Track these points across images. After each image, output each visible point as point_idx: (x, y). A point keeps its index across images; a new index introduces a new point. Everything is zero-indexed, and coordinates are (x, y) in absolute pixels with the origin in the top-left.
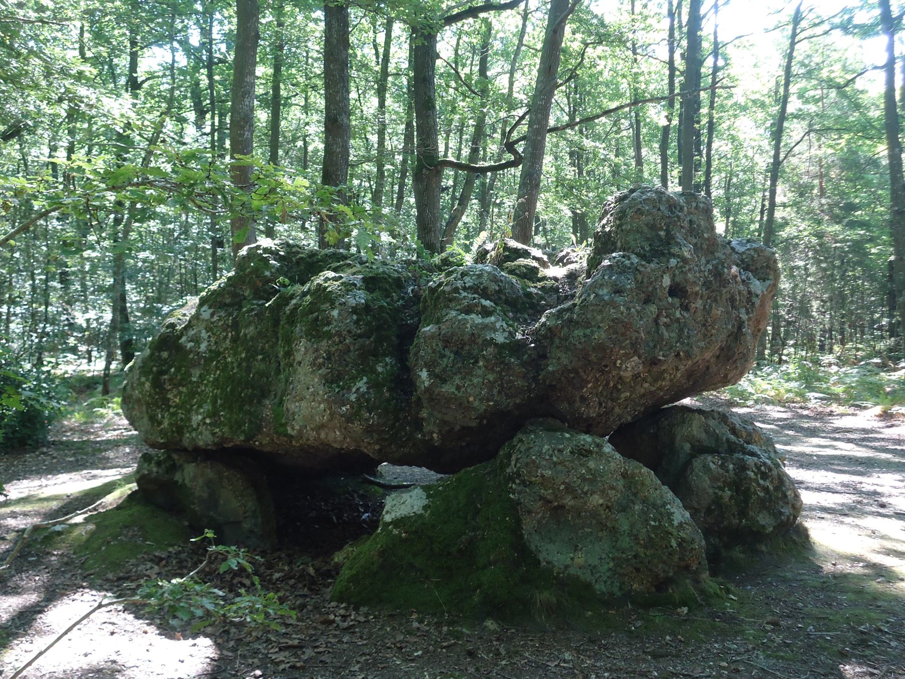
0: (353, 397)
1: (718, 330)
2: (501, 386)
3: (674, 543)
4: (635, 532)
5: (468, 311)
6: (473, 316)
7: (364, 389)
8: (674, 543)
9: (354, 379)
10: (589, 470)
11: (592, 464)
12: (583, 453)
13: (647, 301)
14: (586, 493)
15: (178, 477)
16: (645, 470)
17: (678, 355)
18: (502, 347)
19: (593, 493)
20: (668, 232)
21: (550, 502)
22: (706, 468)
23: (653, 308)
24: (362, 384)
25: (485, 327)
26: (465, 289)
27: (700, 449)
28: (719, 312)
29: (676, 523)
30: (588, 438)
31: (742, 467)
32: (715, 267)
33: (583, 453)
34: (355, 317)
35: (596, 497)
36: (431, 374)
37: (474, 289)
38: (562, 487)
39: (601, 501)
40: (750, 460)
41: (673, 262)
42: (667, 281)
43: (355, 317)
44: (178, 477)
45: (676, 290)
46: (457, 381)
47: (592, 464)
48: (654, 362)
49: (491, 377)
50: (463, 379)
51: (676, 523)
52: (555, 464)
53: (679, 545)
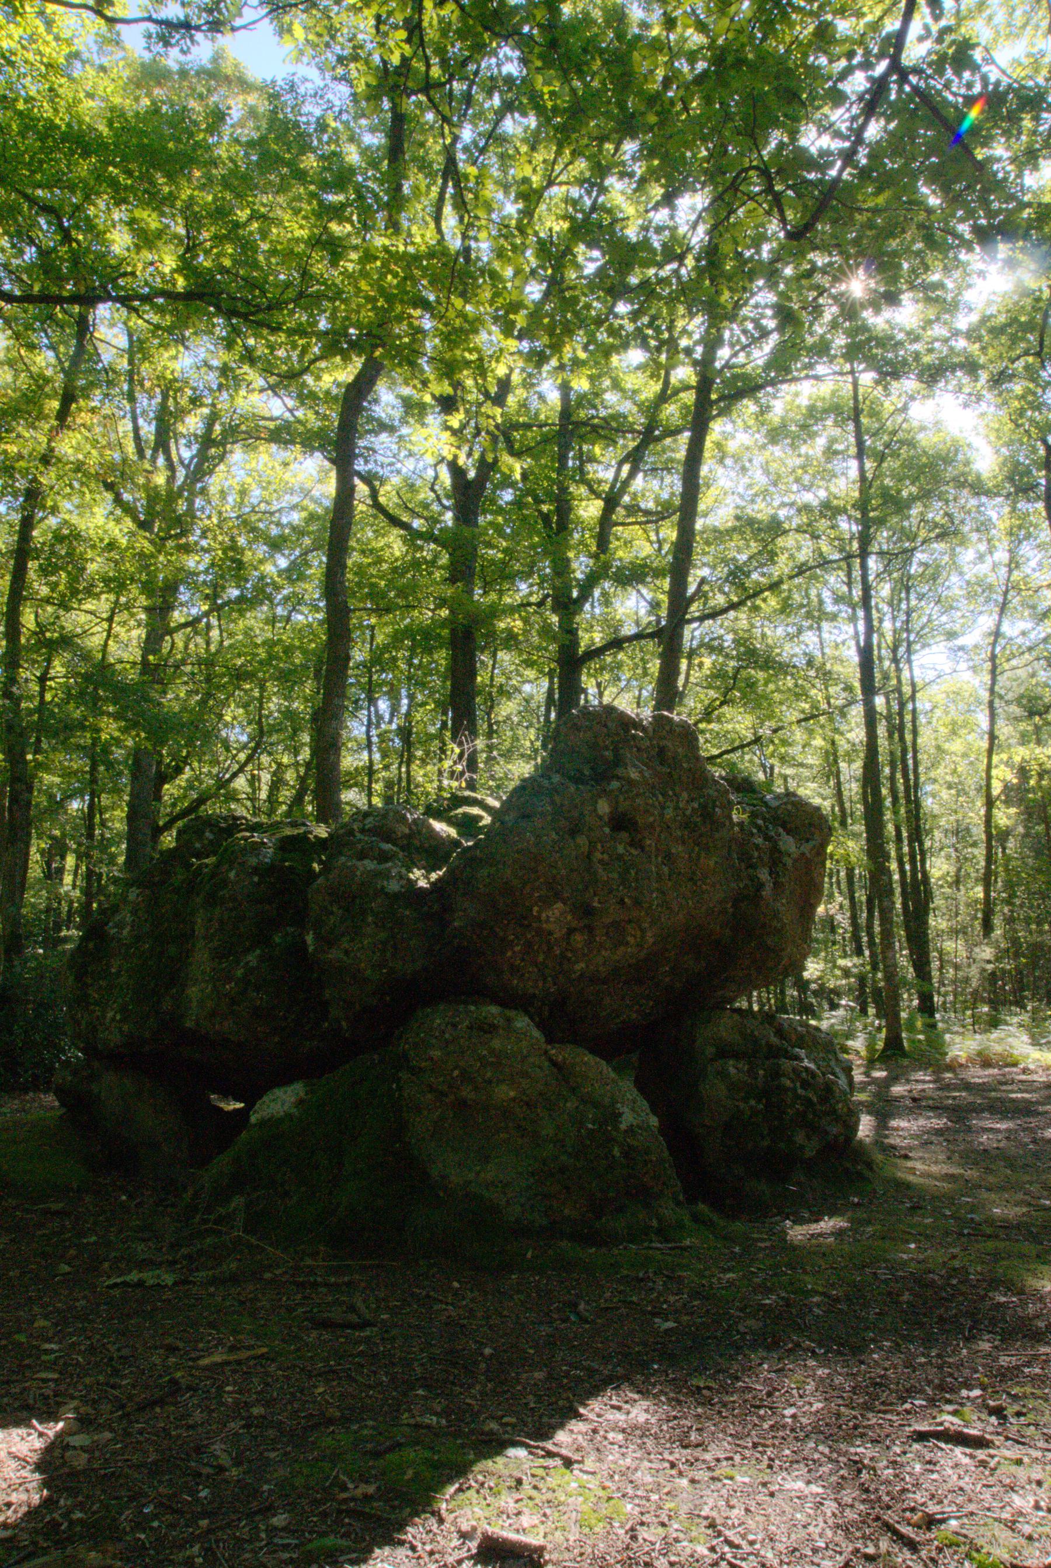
0: (239, 973)
1: (713, 885)
2: (395, 947)
3: (616, 1152)
4: (561, 1136)
5: (362, 856)
6: (366, 862)
7: (254, 963)
8: (616, 1152)
9: (247, 951)
10: (492, 1051)
11: (496, 1044)
12: (487, 1029)
13: (574, 832)
14: (490, 1082)
15: (95, 1087)
16: (588, 1058)
17: (622, 902)
18: (396, 896)
19: (500, 1082)
20: (616, 750)
21: (443, 1094)
22: (723, 1074)
23: (582, 840)
24: (252, 958)
25: (377, 874)
26: (363, 831)
27: (724, 1052)
28: (712, 863)
29: (623, 1126)
30: (494, 1009)
31: (776, 1074)
32: (704, 807)
33: (487, 1029)
34: (256, 879)
35: (504, 1087)
36: (317, 937)
37: (374, 831)
38: (456, 1073)
39: (512, 1094)
40: (786, 1065)
41: (615, 784)
42: (604, 807)
43: (256, 879)
44: (95, 1087)
45: (620, 822)
46: (345, 945)
47: (496, 1044)
48: (588, 911)
49: (383, 935)
50: (352, 940)
51: (623, 1126)
52: (447, 1042)
53: (626, 1155)
